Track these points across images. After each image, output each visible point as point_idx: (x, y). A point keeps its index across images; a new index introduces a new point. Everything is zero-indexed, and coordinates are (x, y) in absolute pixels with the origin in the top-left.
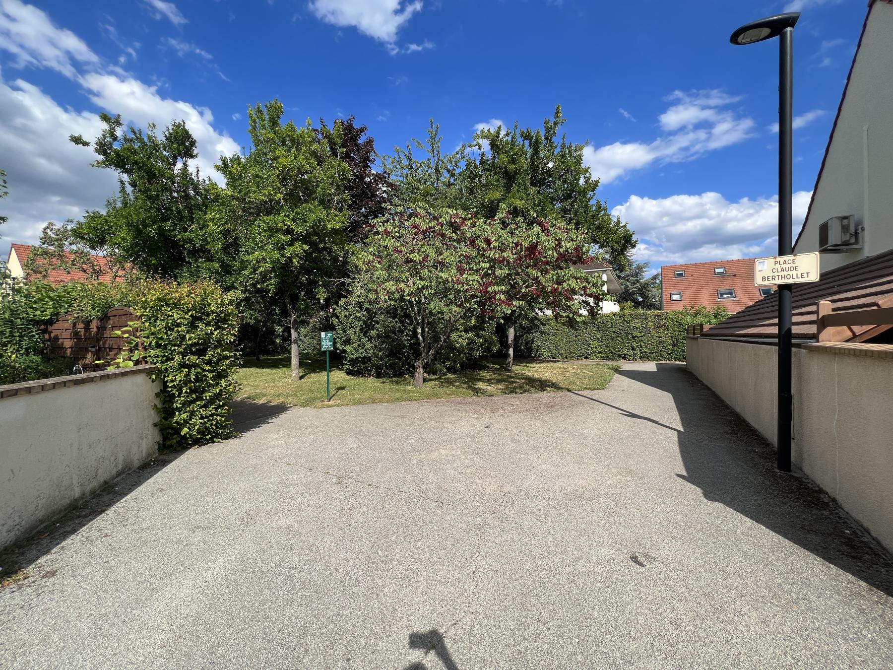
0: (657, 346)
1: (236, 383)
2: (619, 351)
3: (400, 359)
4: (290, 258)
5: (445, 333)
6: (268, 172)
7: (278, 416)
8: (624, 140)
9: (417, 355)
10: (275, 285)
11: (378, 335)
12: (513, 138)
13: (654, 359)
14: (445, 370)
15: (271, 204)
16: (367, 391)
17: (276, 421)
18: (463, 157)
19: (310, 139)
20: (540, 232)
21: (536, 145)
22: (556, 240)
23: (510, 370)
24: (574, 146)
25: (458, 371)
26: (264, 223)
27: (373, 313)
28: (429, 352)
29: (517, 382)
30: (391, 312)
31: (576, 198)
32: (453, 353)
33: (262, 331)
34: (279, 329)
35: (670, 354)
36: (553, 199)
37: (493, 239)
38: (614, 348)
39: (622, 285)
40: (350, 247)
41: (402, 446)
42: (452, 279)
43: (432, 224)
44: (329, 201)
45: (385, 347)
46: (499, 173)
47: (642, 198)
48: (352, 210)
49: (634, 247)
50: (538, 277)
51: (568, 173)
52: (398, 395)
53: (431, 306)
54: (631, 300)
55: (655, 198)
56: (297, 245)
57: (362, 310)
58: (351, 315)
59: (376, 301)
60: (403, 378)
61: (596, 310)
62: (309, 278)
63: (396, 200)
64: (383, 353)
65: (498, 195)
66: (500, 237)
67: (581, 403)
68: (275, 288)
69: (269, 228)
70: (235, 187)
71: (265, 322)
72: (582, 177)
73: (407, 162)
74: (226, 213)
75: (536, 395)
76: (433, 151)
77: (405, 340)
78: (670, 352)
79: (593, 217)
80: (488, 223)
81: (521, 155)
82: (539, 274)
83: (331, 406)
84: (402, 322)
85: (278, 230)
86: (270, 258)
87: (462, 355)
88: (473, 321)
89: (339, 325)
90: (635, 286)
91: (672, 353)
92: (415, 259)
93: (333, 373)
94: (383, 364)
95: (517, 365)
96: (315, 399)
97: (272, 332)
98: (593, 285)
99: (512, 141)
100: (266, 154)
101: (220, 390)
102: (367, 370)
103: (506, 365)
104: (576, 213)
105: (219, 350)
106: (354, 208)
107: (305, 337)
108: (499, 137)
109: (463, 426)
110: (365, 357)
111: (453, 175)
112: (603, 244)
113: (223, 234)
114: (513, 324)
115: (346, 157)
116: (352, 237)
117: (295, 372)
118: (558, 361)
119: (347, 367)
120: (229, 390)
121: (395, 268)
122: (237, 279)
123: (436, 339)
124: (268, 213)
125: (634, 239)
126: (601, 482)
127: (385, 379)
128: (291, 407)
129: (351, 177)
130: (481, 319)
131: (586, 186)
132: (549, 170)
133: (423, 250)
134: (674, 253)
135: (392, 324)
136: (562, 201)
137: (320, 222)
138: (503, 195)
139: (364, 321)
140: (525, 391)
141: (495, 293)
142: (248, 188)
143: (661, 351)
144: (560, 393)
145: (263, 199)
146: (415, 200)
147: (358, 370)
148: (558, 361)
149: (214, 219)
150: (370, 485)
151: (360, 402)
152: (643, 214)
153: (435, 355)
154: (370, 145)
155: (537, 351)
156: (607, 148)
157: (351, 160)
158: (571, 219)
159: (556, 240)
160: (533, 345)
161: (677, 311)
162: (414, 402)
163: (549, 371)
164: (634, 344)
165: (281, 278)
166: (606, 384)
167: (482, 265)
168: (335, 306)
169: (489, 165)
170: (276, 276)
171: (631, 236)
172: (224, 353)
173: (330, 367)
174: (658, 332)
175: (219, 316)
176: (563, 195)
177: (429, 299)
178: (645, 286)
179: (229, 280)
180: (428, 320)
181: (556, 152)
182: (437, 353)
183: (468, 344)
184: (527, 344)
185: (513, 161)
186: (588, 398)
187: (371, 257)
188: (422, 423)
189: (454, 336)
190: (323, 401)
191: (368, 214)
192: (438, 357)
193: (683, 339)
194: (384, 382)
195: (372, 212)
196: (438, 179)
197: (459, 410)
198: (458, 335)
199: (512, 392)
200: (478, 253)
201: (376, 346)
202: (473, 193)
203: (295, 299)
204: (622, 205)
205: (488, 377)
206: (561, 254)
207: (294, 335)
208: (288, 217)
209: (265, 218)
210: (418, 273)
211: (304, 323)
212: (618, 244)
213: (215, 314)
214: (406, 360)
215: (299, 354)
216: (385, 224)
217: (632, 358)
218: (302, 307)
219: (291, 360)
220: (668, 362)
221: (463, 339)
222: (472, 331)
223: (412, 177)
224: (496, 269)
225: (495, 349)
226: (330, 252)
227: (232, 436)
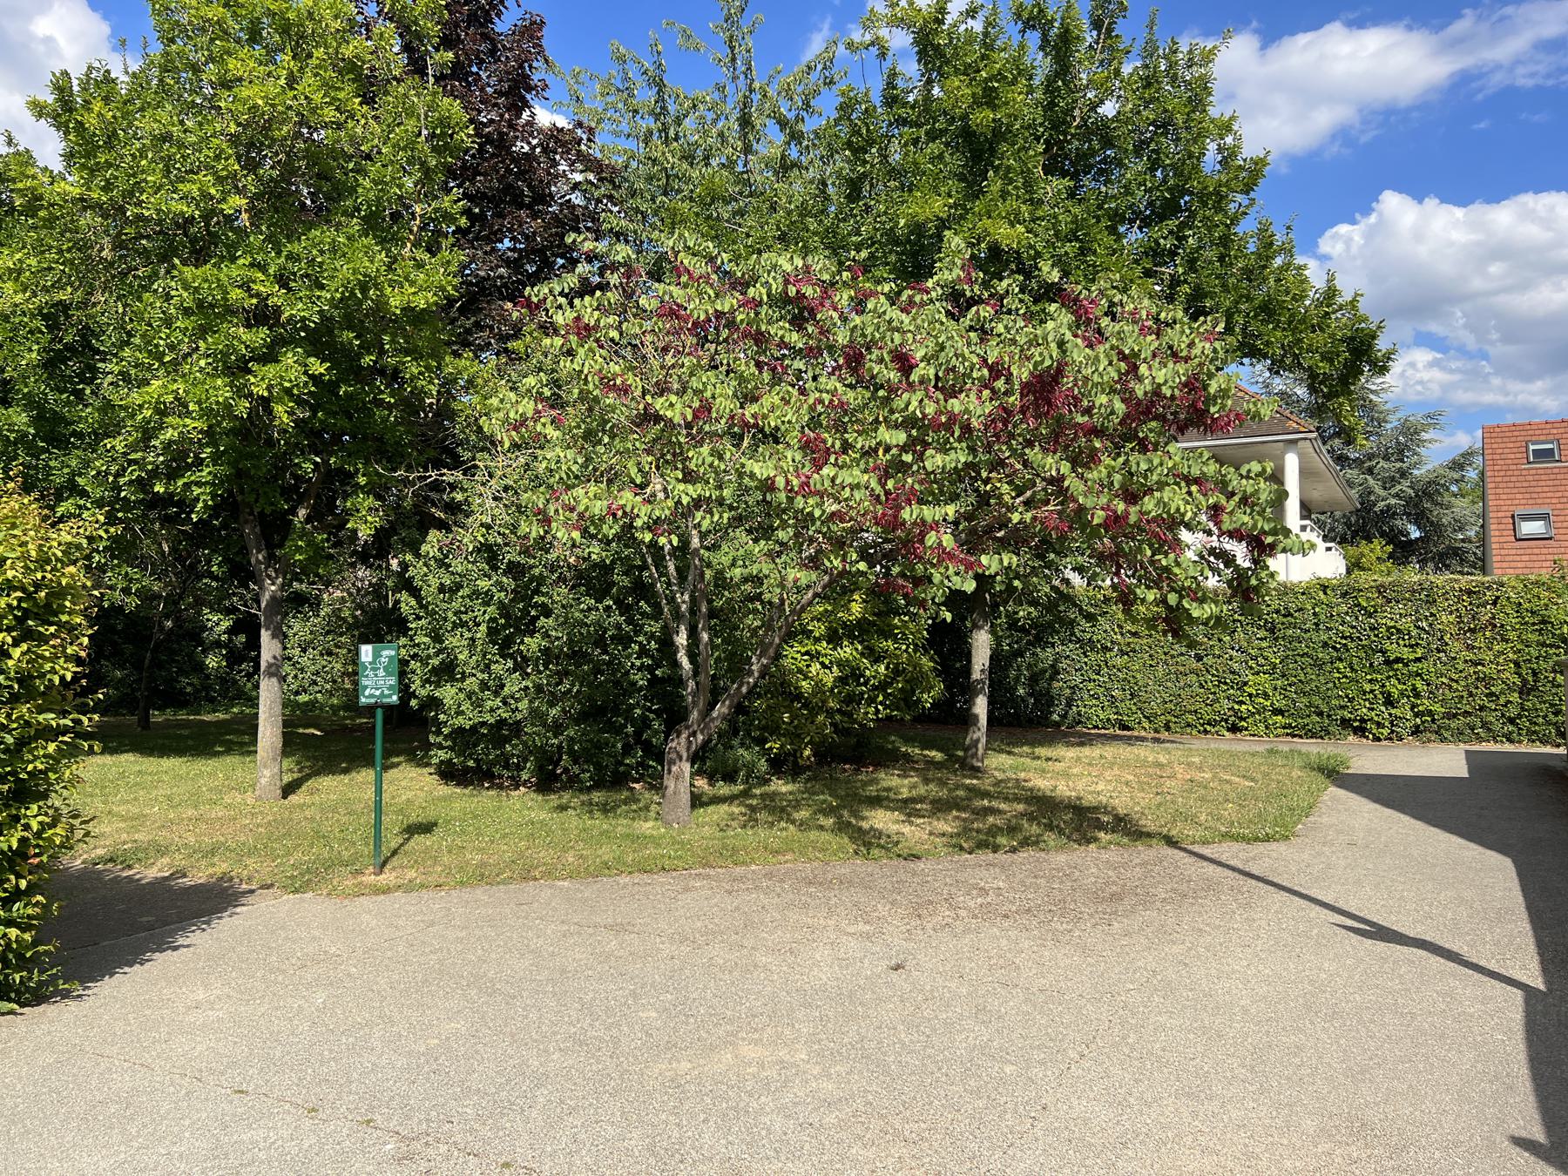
0: (1471, 694)
1: (75, 817)
2: (1342, 707)
3: (618, 730)
4: (265, 402)
5: (764, 648)
6: (200, 124)
7: (208, 923)
8: (1351, 16)
9: (675, 718)
10: (213, 484)
11: (546, 652)
12: (988, 24)
13: (1459, 736)
14: (763, 765)
15: (207, 225)
16: (504, 836)
17: (201, 942)
18: (830, 82)
19: (337, 25)
20: (1068, 336)
21: (1061, 47)
22: (1123, 357)
23: (977, 770)
24: (1185, 49)
25: (809, 768)
26: (186, 289)
27: (531, 580)
28: (713, 708)
29: (999, 812)
30: (593, 580)
31: (1193, 215)
32: (789, 709)
33: (162, 628)
34: (217, 624)
35: (1512, 721)
36: (1117, 218)
37: (919, 355)
38: (1326, 699)
39: (1350, 484)
40: (462, 365)
41: (614, 1032)
42: (788, 482)
43: (725, 305)
44: (396, 216)
45: (570, 691)
46: (943, 132)
47: (1420, 201)
48: (471, 242)
49: (1383, 370)
50: (1063, 478)
51: (1165, 134)
52: (606, 852)
53: (722, 558)
54: (1383, 534)
55: (1462, 202)
56: (289, 359)
57: (495, 568)
58: (459, 586)
59: (543, 544)
60: (625, 794)
61: (1254, 582)
62: (326, 462)
63: (614, 218)
64: (564, 710)
65: (938, 206)
66: (942, 348)
67: (1210, 886)
68: (214, 496)
69: (200, 304)
70: (92, 171)
71: (173, 601)
72: (1212, 147)
73: (652, 94)
74: (60, 252)
75: (1061, 858)
76: (734, 60)
77: (633, 663)
78: (1513, 711)
79: (1248, 273)
80: (904, 297)
81: (1015, 78)
82: (1065, 468)
83: (386, 891)
84: (624, 609)
85: (230, 311)
86: (199, 403)
87: (820, 718)
88: (856, 608)
89: (419, 618)
90: (1393, 491)
91: (1520, 716)
92: (669, 414)
93: (392, 773)
94: (560, 747)
95: (1001, 751)
96: (329, 865)
97: (194, 633)
98: (1244, 501)
99: (986, 34)
100: (195, 69)
101: (23, 841)
102: (507, 766)
103: (966, 750)
104: (1191, 264)
105: (24, 709)
106: (477, 238)
107: (304, 651)
108: (941, 22)
109: (817, 964)
110: (502, 722)
111: (796, 137)
112: (1282, 361)
113: (45, 317)
114: (985, 617)
115: (453, 76)
116: (468, 332)
117: (267, 773)
118: (1139, 739)
119: (443, 755)
120: (50, 839)
121: (606, 440)
122: (87, 464)
123: (736, 665)
124: (199, 256)
125: (1382, 344)
126: (1264, 1164)
127: (566, 796)
128: (252, 892)
129: (468, 143)
130: (881, 596)
131: (1224, 178)
132: (1104, 123)
133: (695, 383)
134: (1528, 378)
135: (593, 616)
136: (1146, 223)
137: (364, 290)
138: (955, 206)
139: (501, 606)
140: (1026, 843)
141: (924, 527)
142: (134, 175)
143: (1482, 708)
144: (1143, 853)
145: (182, 213)
146: (673, 222)
147: (479, 767)
148: (1139, 739)
149: (20, 272)
150: (506, 1165)
151: (483, 877)
152: (1423, 251)
153: (731, 720)
154: (532, 37)
155: (1069, 705)
156: (1303, 39)
157: (469, 84)
158: (1175, 282)
159: (1123, 357)
160: (1056, 684)
161: (1533, 577)
162: (661, 878)
163: (1108, 774)
164: (1394, 688)
165: (232, 464)
166: (1296, 824)
167: (885, 434)
168: (409, 557)
169: (913, 107)
170: (216, 458)
171: (1374, 337)
172: (41, 718)
173: (387, 754)
174: (1470, 648)
175: (29, 596)
176: (1151, 204)
177: (721, 534)
178: (1429, 492)
179: (60, 466)
180: (710, 602)
181: (1127, 70)
182: (739, 709)
183: (842, 680)
184: (1034, 679)
185: (989, 98)
186: (1233, 869)
187: (528, 407)
188: (685, 949)
189: (793, 654)
190: (359, 872)
191: (521, 257)
192: (740, 723)
193: (1554, 671)
194: (563, 808)
195: (534, 251)
196: (747, 150)
197: (806, 906)
198: (807, 653)
199: (982, 845)
200: (874, 397)
201: (539, 689)
202: (859, 198)
203: (275, 530)
204: (1353, 222)
205: (905, 793)
206: (1139, 402)
207: (269, 648)
208: (263, 268)
209: (189, 272)
210: (680, 456)
211: (298, 603)
212: (1331, 361)
213: (19, 594)
214: (638, 734)
215: (285, 706)
216: (577, 302)
217: (1386, 732)
218: (298, 557)
219: (256, 726)
220: (1508, 747)
221: (822, 664)
222: (852, 638)
223: (667, 142)
224: (930, 452)
225: (927, 699)
226: (394, 375)
227: (53, 995)
